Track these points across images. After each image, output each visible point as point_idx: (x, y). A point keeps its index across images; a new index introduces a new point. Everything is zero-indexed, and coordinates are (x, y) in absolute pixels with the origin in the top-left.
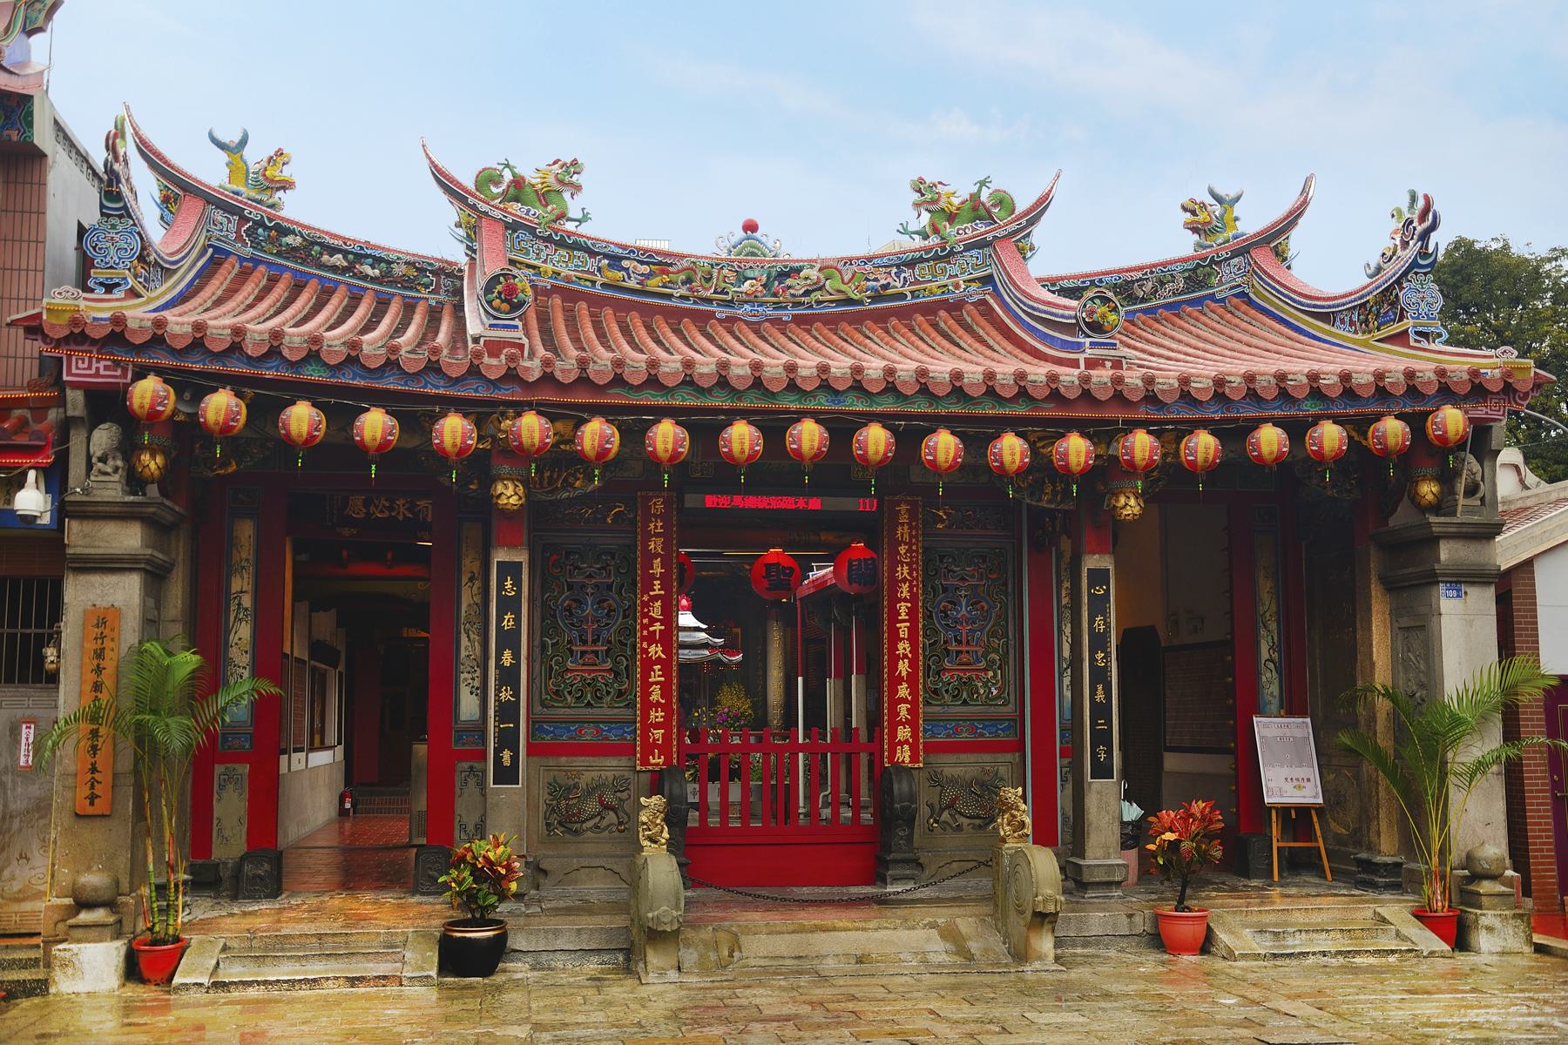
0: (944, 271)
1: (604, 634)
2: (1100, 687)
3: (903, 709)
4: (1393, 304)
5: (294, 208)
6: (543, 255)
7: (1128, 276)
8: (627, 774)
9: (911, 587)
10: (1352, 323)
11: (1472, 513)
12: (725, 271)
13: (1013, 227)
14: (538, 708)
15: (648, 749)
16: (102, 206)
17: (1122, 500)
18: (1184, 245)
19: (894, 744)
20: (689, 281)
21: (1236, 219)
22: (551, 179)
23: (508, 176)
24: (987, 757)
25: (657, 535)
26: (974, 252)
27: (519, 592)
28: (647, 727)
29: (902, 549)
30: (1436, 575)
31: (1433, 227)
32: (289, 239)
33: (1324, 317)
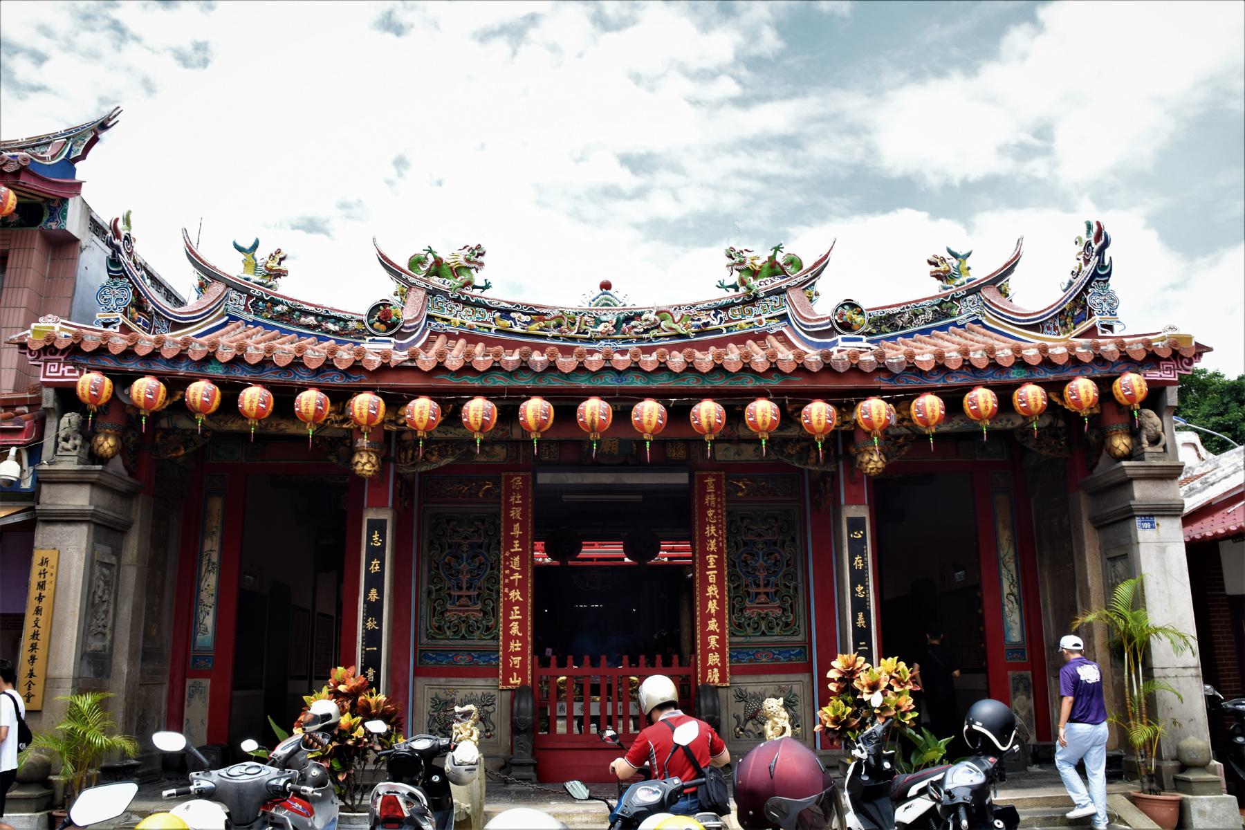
0: (750, 312)
1: (477, 583)
2: (860, 615)
3: (713, 640)
4: (1084, 307)
5: (285, 288)
6: (454, 312)
7: (890, 311)
8: (492, 692)
9: (717, 543)
10: (1055, 328)
11: (1158, 458)
12: (586, 318)
13: (802, 279)
14: (424, 640)
15: (508, 672)
16: (109, 271)
17: (867, 458)
18: (934, 288)
19: (706, 669)
20: (559, 325)
21: (969, 268)
22: (461, 259)
23: (431, 259)
24: (782, 677)
25: (517, 505)
26: (772, 298)
27: (384, 543)
28: (508, 655)
29: (710, 513)
30: (1131, 510)
31: (1106, 244)
32: (279, 308)
33: (1035, 328)
